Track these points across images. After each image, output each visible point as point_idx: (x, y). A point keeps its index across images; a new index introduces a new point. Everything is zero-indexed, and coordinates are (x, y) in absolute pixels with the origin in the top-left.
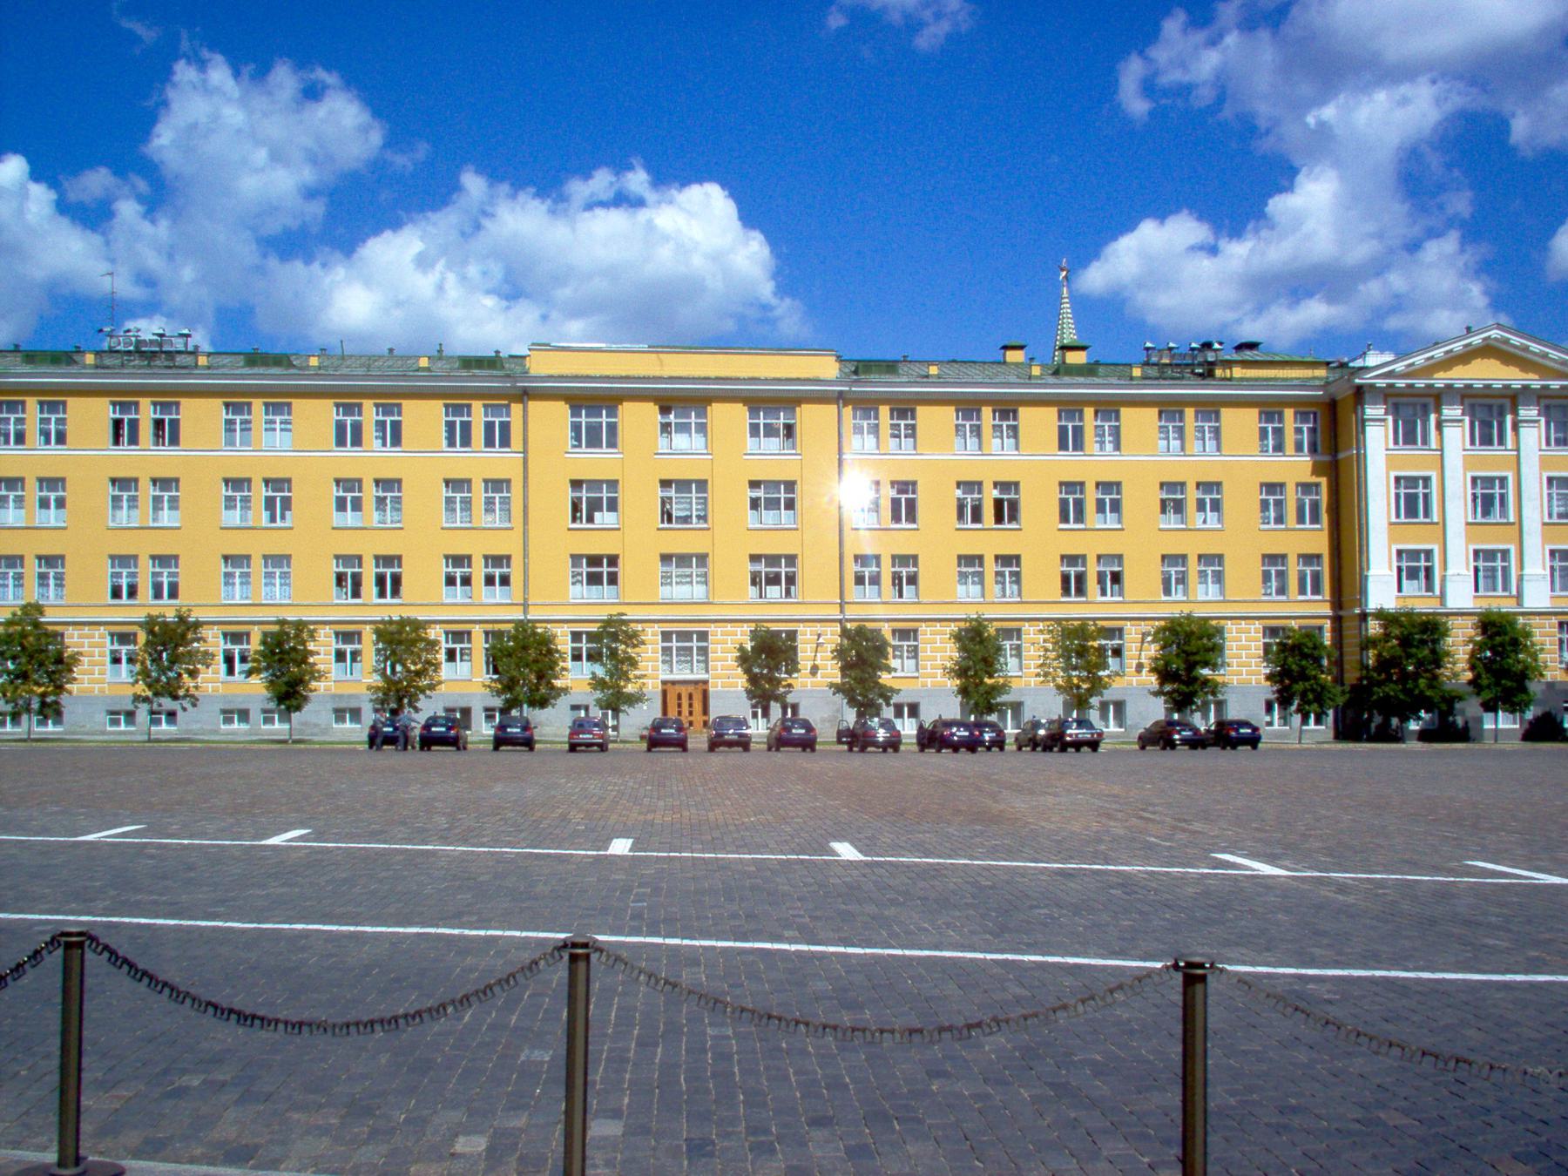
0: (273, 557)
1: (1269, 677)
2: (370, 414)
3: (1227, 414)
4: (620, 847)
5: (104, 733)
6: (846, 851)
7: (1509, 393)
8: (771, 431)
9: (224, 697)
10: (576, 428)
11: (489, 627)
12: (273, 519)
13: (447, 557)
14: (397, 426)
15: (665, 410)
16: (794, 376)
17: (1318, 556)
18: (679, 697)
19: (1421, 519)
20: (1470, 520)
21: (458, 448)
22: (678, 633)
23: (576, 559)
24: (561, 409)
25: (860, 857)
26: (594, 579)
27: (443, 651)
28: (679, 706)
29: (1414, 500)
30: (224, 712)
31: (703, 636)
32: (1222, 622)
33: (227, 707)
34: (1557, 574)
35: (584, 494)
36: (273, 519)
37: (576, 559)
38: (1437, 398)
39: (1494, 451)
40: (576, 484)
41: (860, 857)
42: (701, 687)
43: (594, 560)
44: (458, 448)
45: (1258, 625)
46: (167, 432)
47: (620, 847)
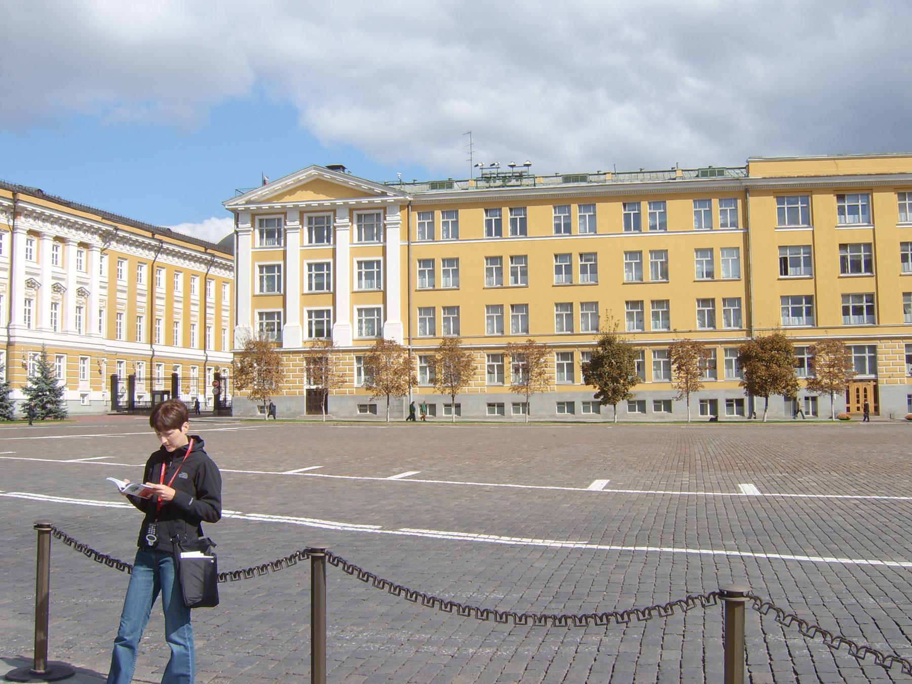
0: (587, 303)
1: (742, 384)
2: (507, 215)
3: (671, 204)
4: (598, 485)
5: (485, 417)
6: (749, 489)
7: (283, 211)
8: (853, 210)
9: (559, 394)
10: (781, 211)
11: (422, 353)
12: (516, 281)
13: (698, 300)
14: (524, 221)
15: (841, 198)
16: (787, 175)
17: (739, 299)
18: (858, 390)
19: (325, 290)
20: (356, 289)
21: (633, 231)
22: (855, 347)
23: (784, 298)
24: (770, 202)
25: (758, 493)
26: (797, 313)
27: (418, 369)
28: (858, 396)
30: (489, 405)
31: (873, 349)
32: (644, 347)
33: (560, 400)
34: (364, 325)
35: (849, 255)
36: (516, 281)
37: (784, 298)
38: (284, 212)
39: (326, 247)
40: (843, 247)
41: (758, 493)
42: (872, 383)
43: (796, 299)
44: (633, 231)
45: (902, 343)
46: (521, 228)
47: (598, 485)
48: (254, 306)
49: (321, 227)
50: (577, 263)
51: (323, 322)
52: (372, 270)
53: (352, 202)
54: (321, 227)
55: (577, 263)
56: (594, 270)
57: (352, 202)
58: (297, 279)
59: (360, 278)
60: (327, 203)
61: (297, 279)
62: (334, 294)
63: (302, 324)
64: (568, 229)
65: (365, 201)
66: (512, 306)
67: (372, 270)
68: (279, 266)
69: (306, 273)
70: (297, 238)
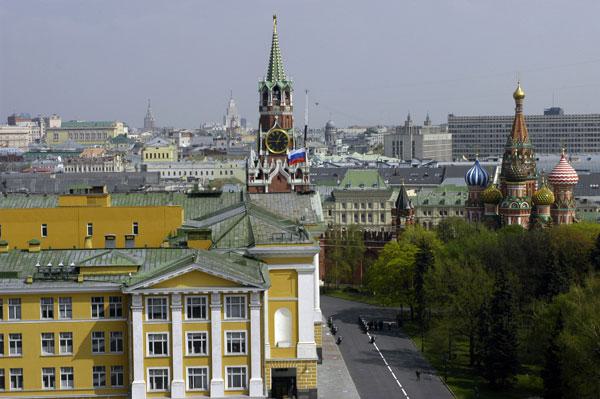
20: (187, 354)
29: (159, 347)
48: (185, 364)
49: (197, 309)
50: (58, 339)
51: (161, 378)
52: (199, 344)
53: (226, 290)
54: (197, 309)
55: (58, 339)
56: (20, 345)
57: (226, 290)
58: (179, 349)
59: (190, 347)
60: (206, 292)
61: (179, 349)
62: (210, 357)
63: (184, 378)
64: (51, 315)
65: (236, 290)
66: (11, 370)
67: (199, 344)
68: (165, 336)
69: (187, 340)
70: (178, 318)
